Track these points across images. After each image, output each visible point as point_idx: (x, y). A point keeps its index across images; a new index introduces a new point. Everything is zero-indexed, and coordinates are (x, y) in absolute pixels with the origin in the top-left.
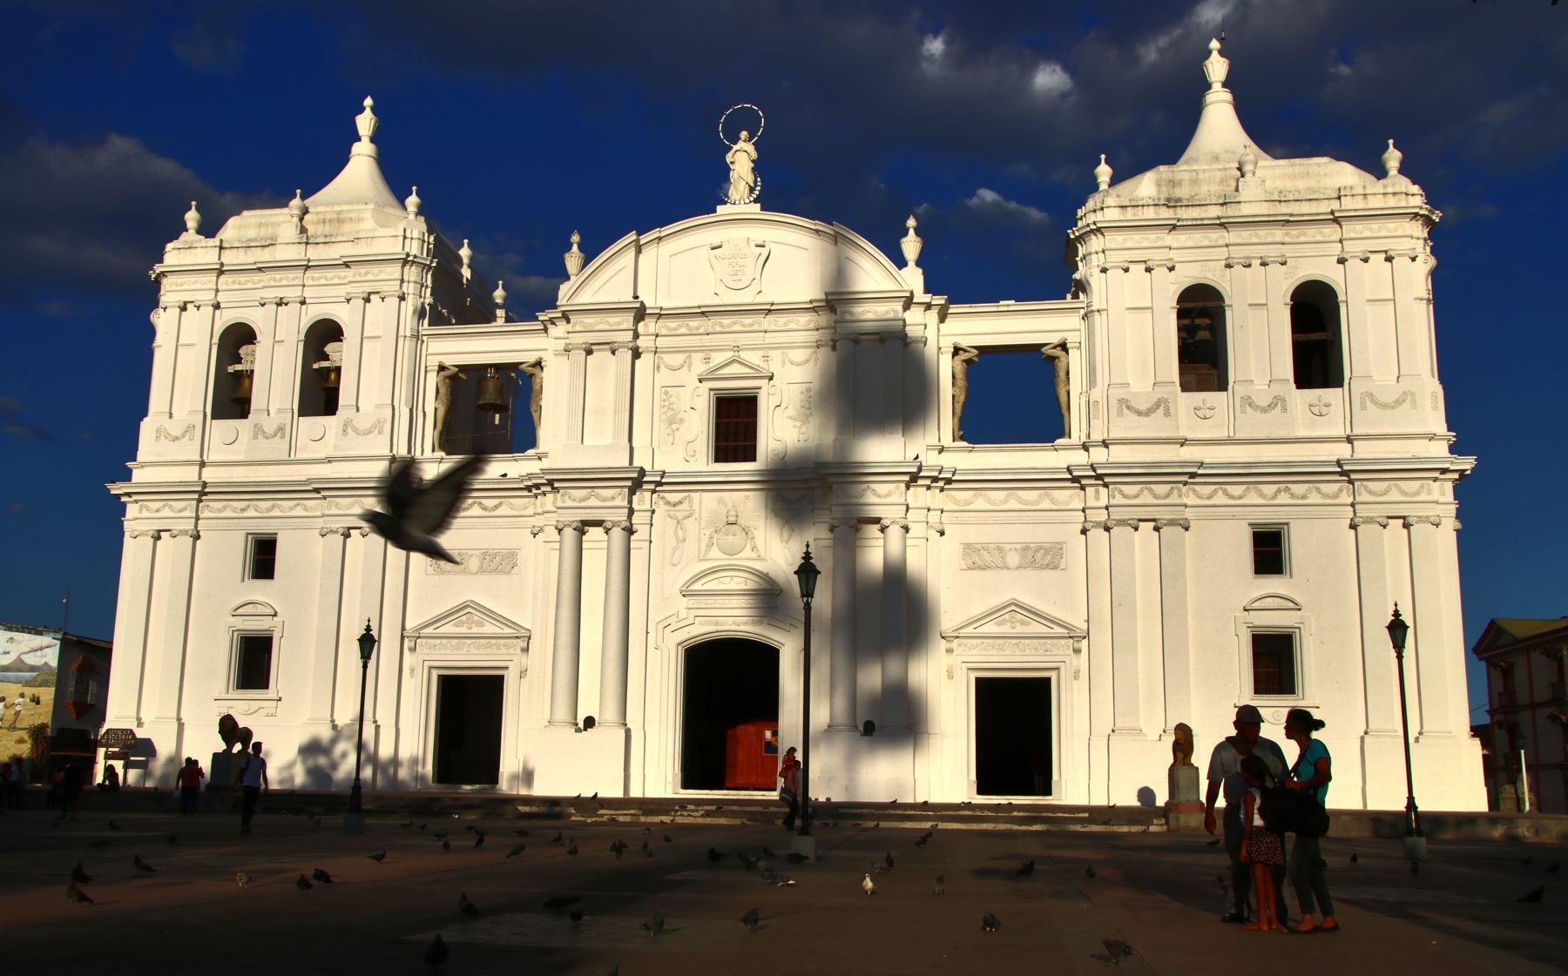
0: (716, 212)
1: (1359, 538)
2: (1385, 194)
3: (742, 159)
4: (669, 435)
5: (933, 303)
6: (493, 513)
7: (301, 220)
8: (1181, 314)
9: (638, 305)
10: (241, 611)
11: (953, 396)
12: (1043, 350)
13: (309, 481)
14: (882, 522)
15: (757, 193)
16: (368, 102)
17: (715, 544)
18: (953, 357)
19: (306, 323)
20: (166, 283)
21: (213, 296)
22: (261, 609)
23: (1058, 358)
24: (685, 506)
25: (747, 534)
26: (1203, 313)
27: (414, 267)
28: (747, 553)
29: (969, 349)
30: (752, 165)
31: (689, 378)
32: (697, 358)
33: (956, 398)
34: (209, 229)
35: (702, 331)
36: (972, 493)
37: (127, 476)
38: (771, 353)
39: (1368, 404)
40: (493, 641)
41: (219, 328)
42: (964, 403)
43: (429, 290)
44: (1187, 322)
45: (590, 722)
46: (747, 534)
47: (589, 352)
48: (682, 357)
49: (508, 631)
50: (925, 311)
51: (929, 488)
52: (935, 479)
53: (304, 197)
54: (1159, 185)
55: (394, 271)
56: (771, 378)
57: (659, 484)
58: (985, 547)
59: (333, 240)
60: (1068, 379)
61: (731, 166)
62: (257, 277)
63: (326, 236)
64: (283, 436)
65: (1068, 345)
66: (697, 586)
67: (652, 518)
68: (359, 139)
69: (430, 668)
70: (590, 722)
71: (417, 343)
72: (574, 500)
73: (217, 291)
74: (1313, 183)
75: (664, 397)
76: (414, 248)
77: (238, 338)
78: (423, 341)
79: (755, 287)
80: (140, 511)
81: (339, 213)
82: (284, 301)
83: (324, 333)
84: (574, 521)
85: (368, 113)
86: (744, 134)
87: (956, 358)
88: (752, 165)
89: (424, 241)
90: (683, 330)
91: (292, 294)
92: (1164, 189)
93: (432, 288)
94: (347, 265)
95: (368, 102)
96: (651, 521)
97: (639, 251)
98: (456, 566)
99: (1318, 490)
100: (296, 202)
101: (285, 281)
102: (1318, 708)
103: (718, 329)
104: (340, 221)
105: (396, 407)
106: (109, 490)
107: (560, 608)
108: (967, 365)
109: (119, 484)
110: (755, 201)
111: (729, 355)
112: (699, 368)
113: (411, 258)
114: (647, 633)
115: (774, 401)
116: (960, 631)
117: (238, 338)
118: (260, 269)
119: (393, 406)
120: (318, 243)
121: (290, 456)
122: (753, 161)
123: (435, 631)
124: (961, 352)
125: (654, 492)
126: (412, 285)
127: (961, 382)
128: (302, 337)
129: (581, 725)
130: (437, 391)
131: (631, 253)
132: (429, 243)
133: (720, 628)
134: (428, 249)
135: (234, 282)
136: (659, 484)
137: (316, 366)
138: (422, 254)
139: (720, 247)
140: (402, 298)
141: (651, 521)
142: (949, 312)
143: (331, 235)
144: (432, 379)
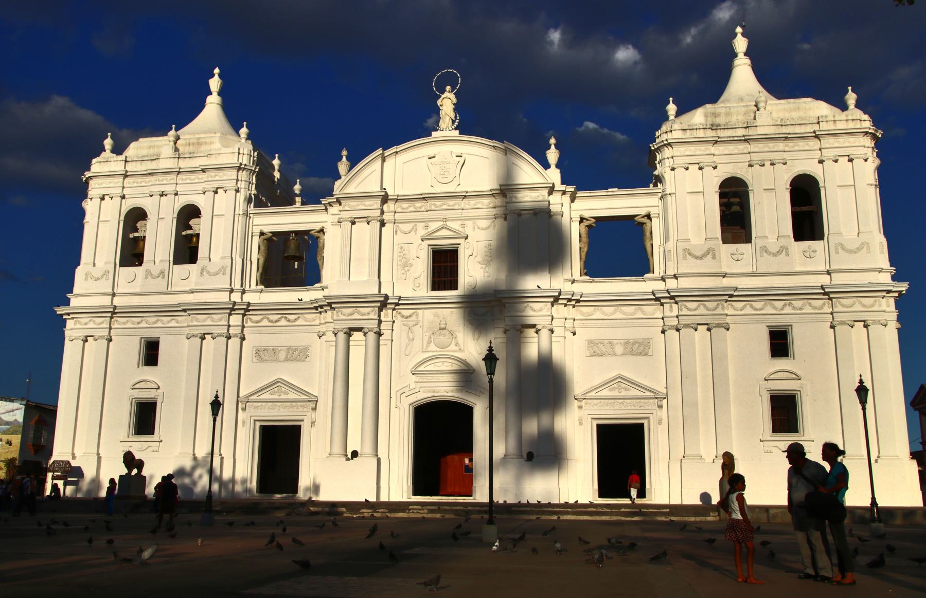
0: (431, 136)
2: (847, 120)
3: (447, 103)
4: (403, 274)
5: (567, 190)
6: (294, 324)
7: (175, 143)
8: (722, 196)
9: (383, 194)
10: (137, 386)
11: (580, 248)
12: (311, 232)
13: (180, 305)
14: (536, 327)
15: (457, 124)
16: (217, 71)
17: (432, 342)
18: (580, 224)
19: (178, 207)
20: (92, 183)
21: (121, 191)
22: (149, 385)
23: (645, 223)
24: (414, 318)
25: (452, 335)
26: (736, 195)
27: (244, 172)
28: (453, 347)
29: (589, 219)
30: (454, 107)
31: (416, 238)
32: (420, 226)
33: (582, 250)
34: (118, 150)
35: (423, 209)
36: (593, 308)
37: (67, 302)
38: (467, 222)
39: (840, 250)
40: (294, 404)
41: (124, 211)
42: (587, 252)
43: (254, 186)
44: (725, 200)
45: (355, 454)
46: (452, 335)
47: (353, 223)
48: (412, 225)
49: (303, 397)
50: (562, 195)
51: (566, 305)
52: (570, 300)
53: (177, 130)
54: (706, 116)
55: (233, 174)
56: (466, 238)
57: (397, 304)
58: (601, 342)
59: (195, 155)
60: (652, 236)
61: (440, 107)
62: (148, 179)
63: (190, 153)
64: (163, 277)
66: (422, 368)
67: (393, 325)
68: (211, 94)
69: (255, 421)
70: (355, 454)
71: (247, 218)
72: (344, 315)
73: (123, 188)
74: (801, 114)
75: (400, 250)
76: (245, 160)
77: (136, 217)
78: (250, 217)
79: (456, 182)
80: (75, 324)
81: (199, 139)
82: (165, 193)
83: (190, 213)
84: (344, 328)
85: (216, 77)
86: (448, 88)
87: (581, 224)
88: (454, 107)
89: (251, 156)
90: (412, 209)
91: (169, 189)
92: (709, 119)
93: (256, 184)
94: (203, 171)
95: (217, 71)
96: (392, 327)
97: (384, 160)
99: (752, 306)
100: (172, 133)
101: (167, 184)
103: (433, 208)
104: (199, 144)
105: (234, 258)
106: (56, 312)
109: (62, 308)
110: (456, 129)
111: (440, 224)
112: (422, 232)
113: (243, 166)
114: (391, 397)
115: (468, 252)
116: (587, 395)
117: (136, 217)
118: (150, 174)
119: (232, 258)
120: (185, 158)
121: (168, 289)
122: (454, 104)
123: (257, 398)
124: (585, 221)
125: (394, 309)
126: (243, 183)
127: (585, 239)
128: (176, 216)
129: (349, 456)
130: (259, 248)
131: (379, 161)
132: (254, 157)
133: (436, 394)
134: (254, 160)
135: (134, 182)
136: (397, 304)
137: (184, 233)
138: (250, 163)
139: (434, 157)
140: (237, 191)
141: (392, 327)
142: (577, 196)
143: (194, 153)
144: (256, 241)
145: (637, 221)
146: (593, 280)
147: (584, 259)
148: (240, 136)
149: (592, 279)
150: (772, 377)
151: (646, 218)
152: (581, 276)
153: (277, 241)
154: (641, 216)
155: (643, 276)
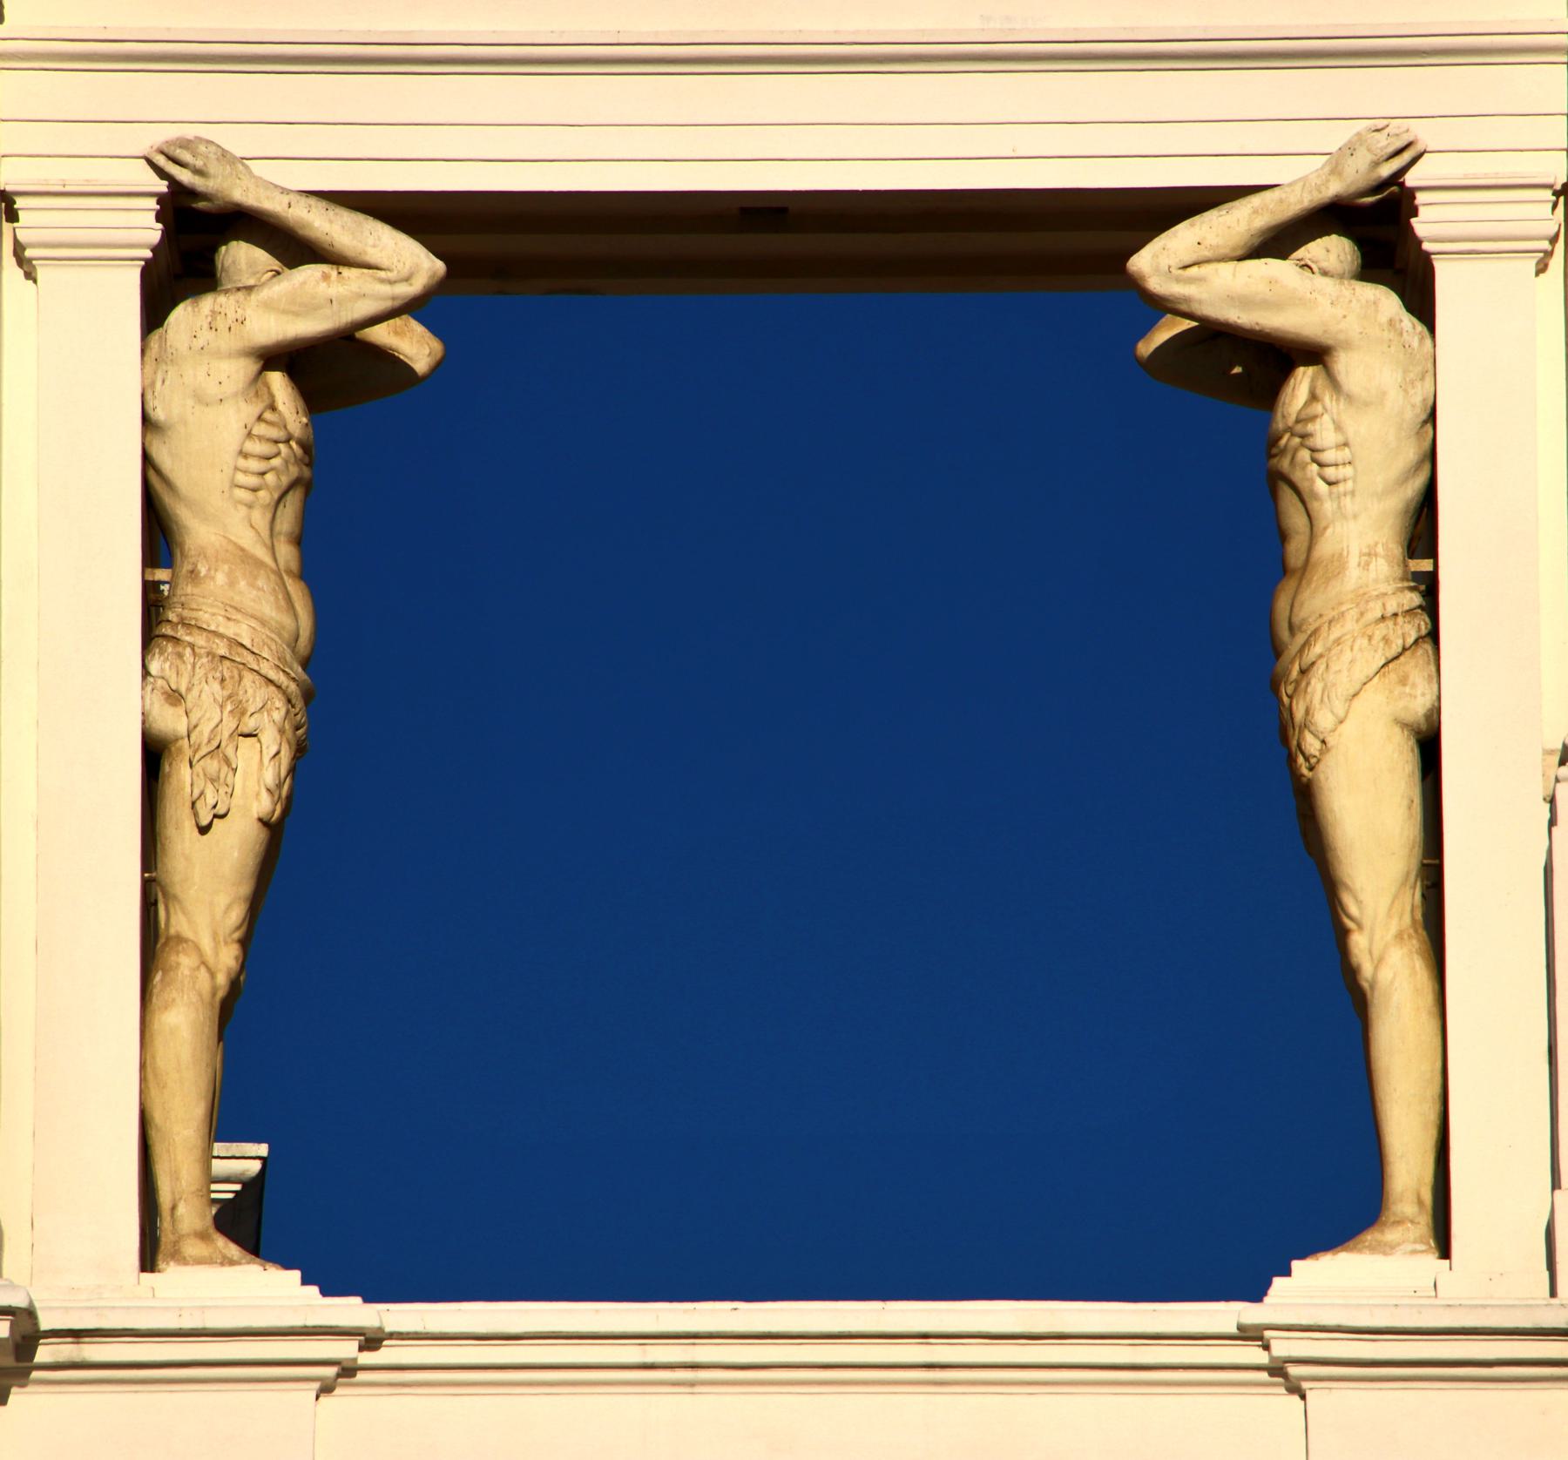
1: (110, 119)
11: (155, 754)
18: (154, 314)
23: (1316, 354)
33: (182, 777)
42: (274, 830)
60: (1429, 587)
65: (1426, 224)
87: (182, 317)
98: (1551, 210)
102: (1451, 1269)
107: (1396, 158)
108: (312, 396)
124: (241, 257)
145: (1160, 307)
146: (371, 1341)
147: (227, 958)
148: (1180, 268)
149: (352, 1311)
150: (1326, 693)
151: (1333, 250)
152: (148, 1261)
153: (3, 202)
154: (1239, 221)
155: (1257, 1293)
